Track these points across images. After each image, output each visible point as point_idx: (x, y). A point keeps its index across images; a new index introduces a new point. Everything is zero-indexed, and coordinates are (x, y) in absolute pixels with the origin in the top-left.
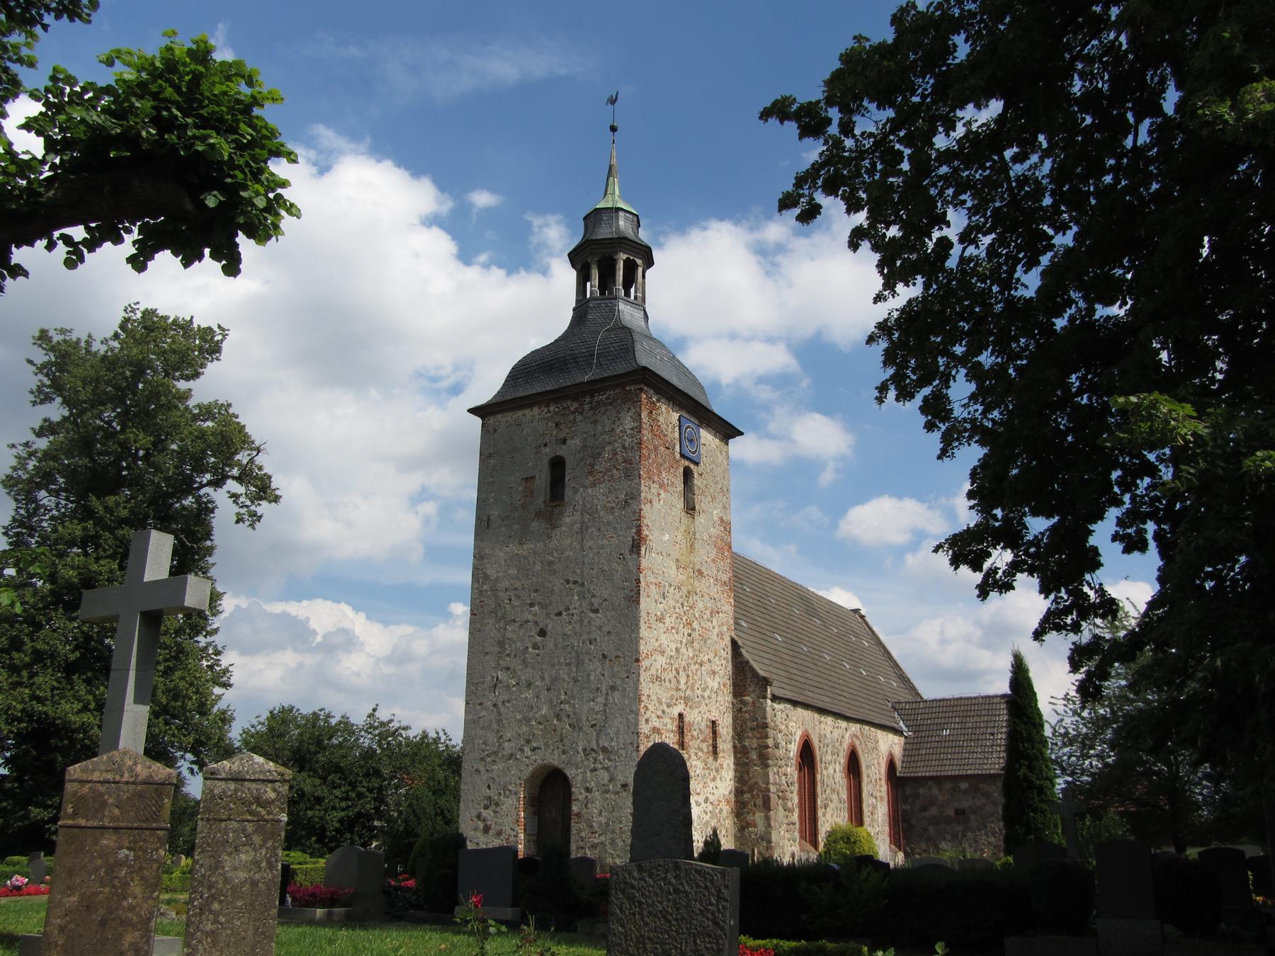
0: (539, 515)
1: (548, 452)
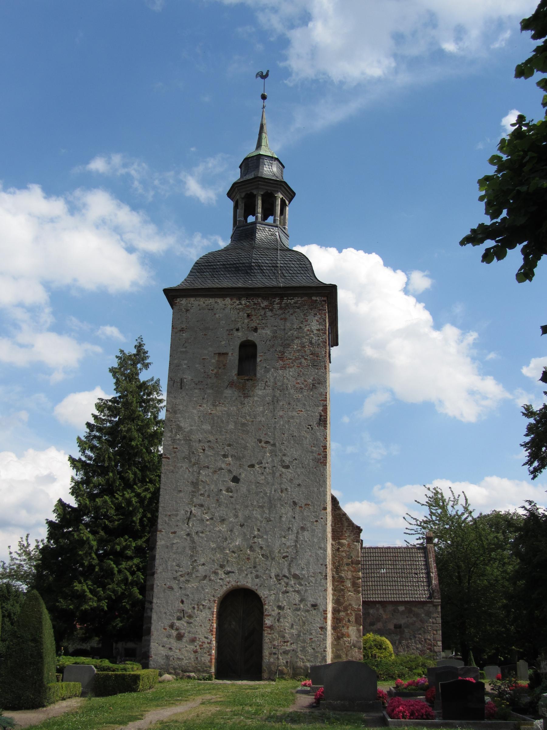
0: (231, 384)
1: (240, 336)
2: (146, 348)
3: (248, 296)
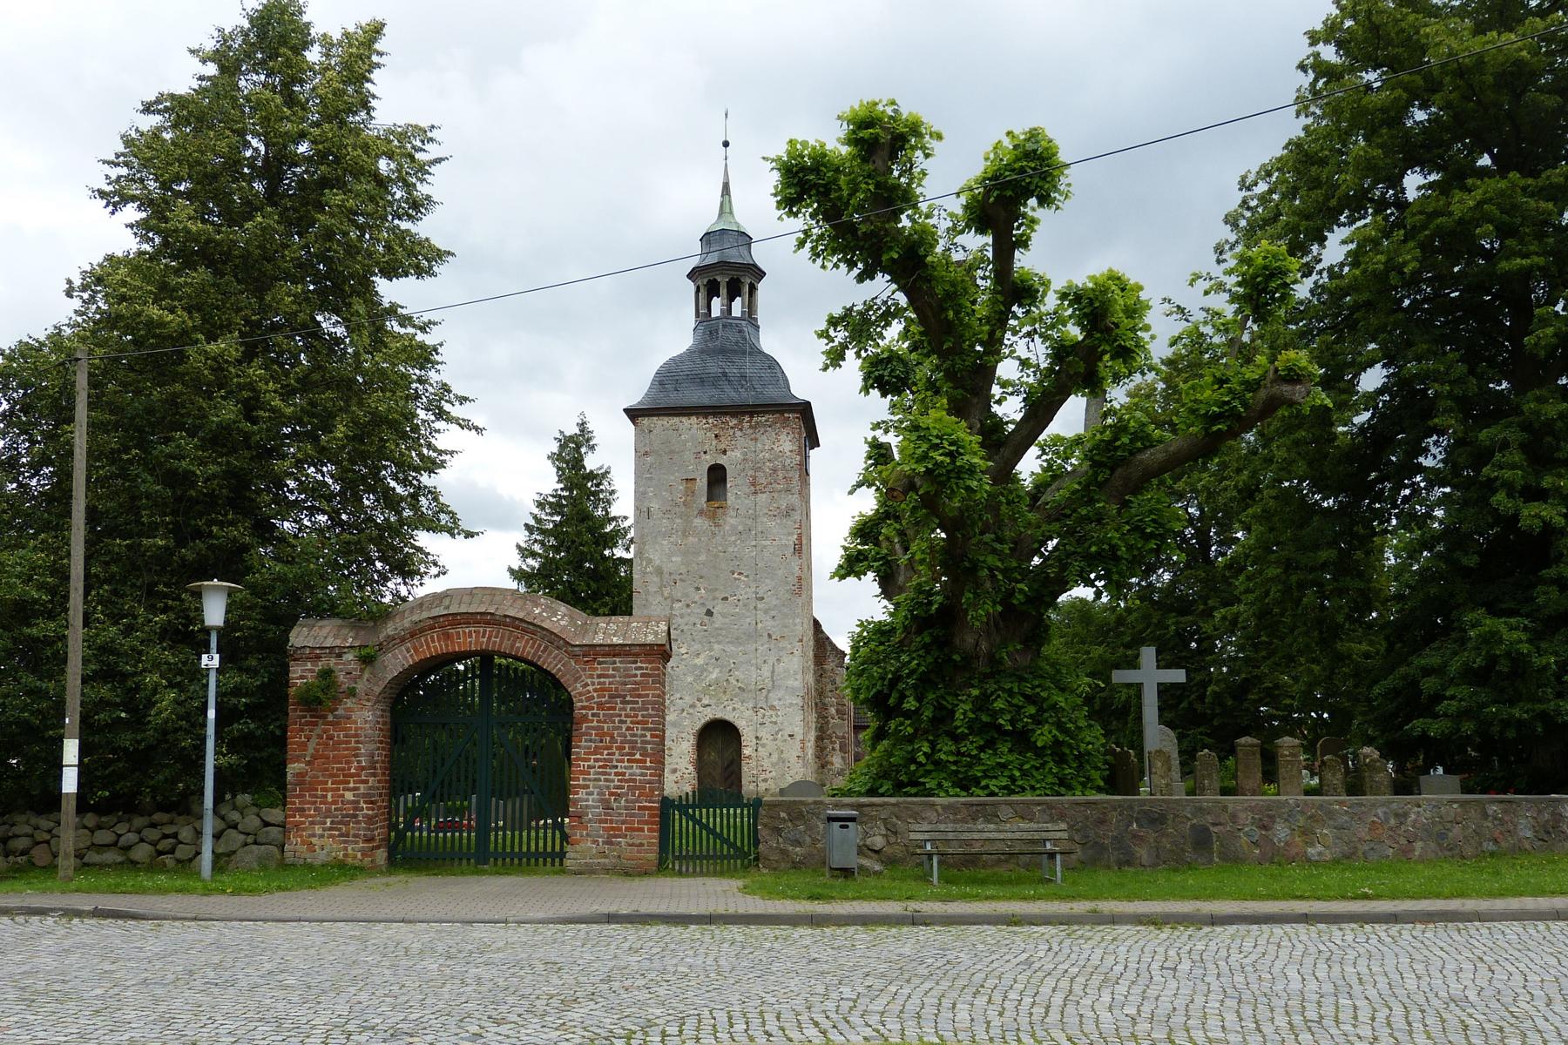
0: (701, 513)
1: (709, 460)
2: (590, 427)
3: (714, 415)
